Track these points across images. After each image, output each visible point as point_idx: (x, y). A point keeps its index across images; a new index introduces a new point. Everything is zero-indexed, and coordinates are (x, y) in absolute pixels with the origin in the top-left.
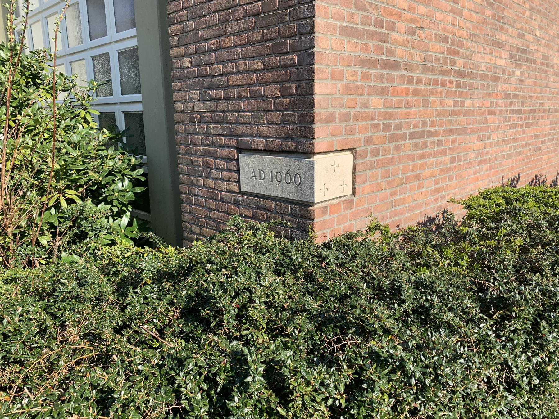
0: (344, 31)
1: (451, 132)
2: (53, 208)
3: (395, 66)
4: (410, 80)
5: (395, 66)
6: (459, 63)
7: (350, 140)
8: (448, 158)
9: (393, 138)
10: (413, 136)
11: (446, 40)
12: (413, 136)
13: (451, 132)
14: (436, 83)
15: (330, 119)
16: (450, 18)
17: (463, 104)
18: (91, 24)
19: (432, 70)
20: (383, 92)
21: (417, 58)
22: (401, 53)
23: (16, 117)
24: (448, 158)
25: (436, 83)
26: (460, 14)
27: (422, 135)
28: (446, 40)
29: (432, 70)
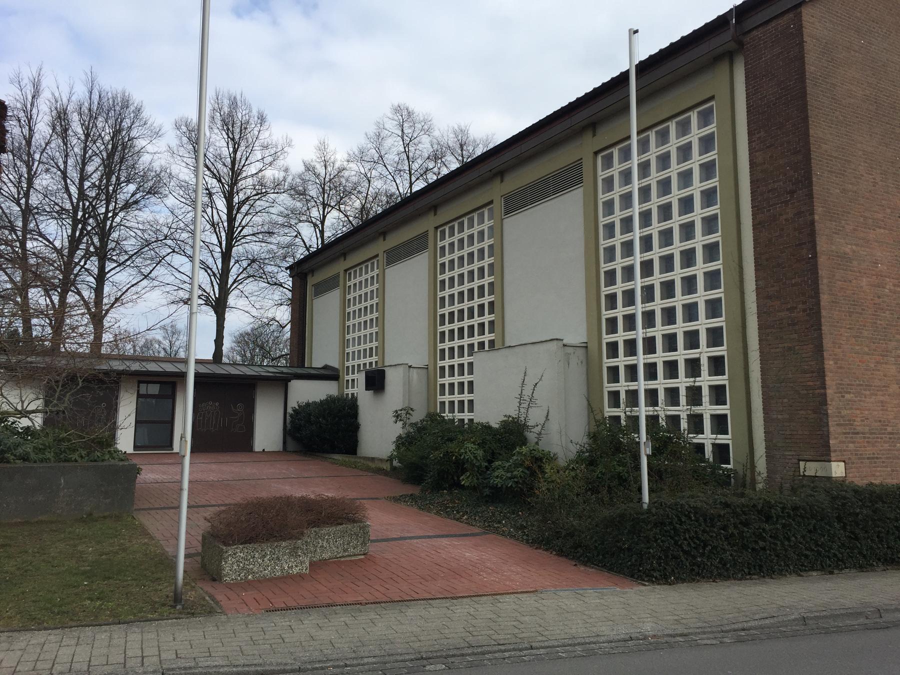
0: (837, 425)
1: (890, 458)
2: (258, 446)
3: (858, 433)
4: (864, 438)
5: (858, 433)
6: (889, 429)
7: (843, 458)
8: (889, 469)
9: (859, 459)
10: (868, 458)
11: (880, 421)
12: (868, 458)
13: (890, 458)
14: (877, 438)
15: (835, 451)
16: (881, 412)
17: (895, 446)
18: (739, 319)
19: (875, 433)
20: (853, 442)
21: (867, 429)
22: (859, 429)
23: (699, 389)
24: (889, 469)
25: (877, 438)
26: (887, 410)
27: (873, 458)
28: (880, 421)
29: (875, 433)
